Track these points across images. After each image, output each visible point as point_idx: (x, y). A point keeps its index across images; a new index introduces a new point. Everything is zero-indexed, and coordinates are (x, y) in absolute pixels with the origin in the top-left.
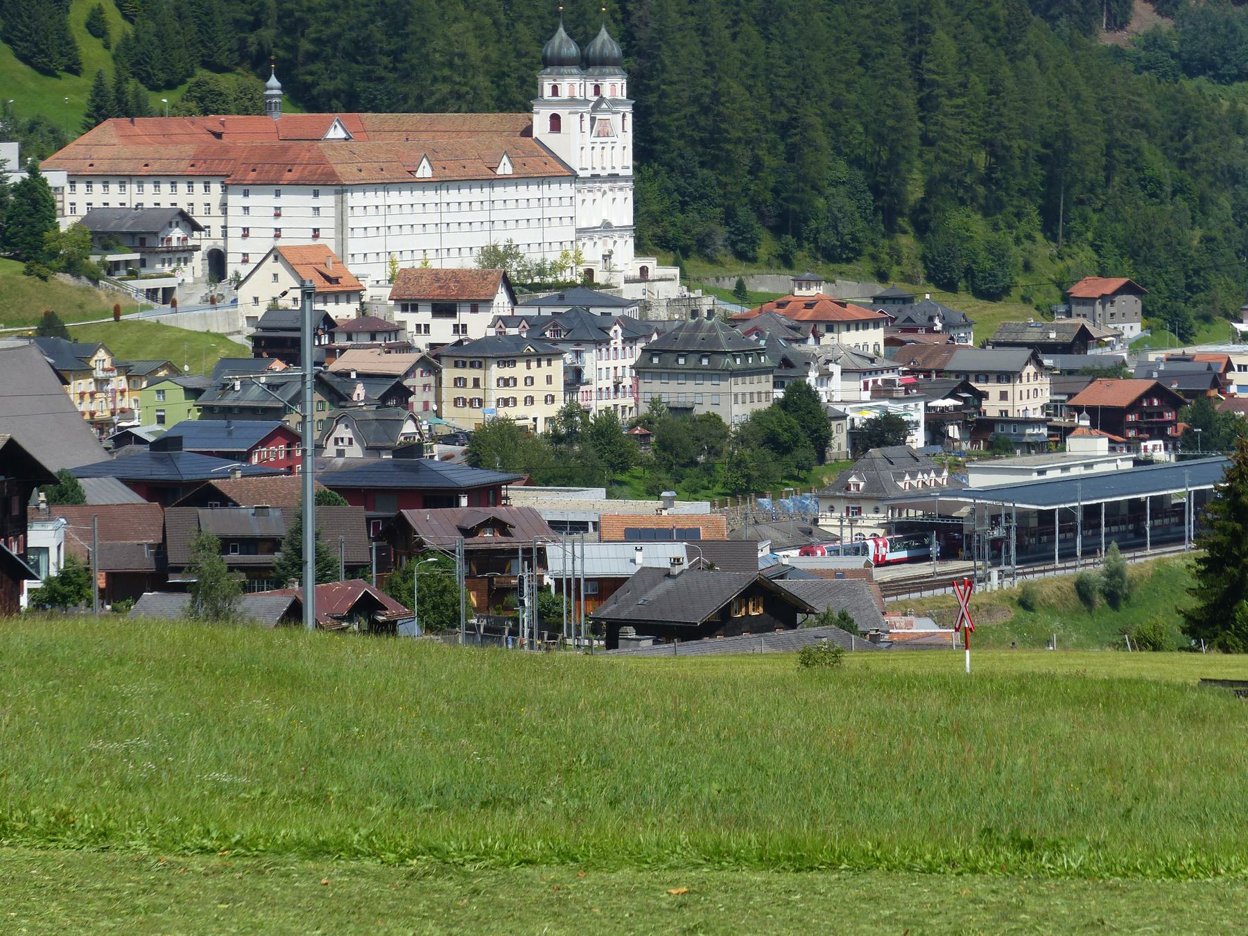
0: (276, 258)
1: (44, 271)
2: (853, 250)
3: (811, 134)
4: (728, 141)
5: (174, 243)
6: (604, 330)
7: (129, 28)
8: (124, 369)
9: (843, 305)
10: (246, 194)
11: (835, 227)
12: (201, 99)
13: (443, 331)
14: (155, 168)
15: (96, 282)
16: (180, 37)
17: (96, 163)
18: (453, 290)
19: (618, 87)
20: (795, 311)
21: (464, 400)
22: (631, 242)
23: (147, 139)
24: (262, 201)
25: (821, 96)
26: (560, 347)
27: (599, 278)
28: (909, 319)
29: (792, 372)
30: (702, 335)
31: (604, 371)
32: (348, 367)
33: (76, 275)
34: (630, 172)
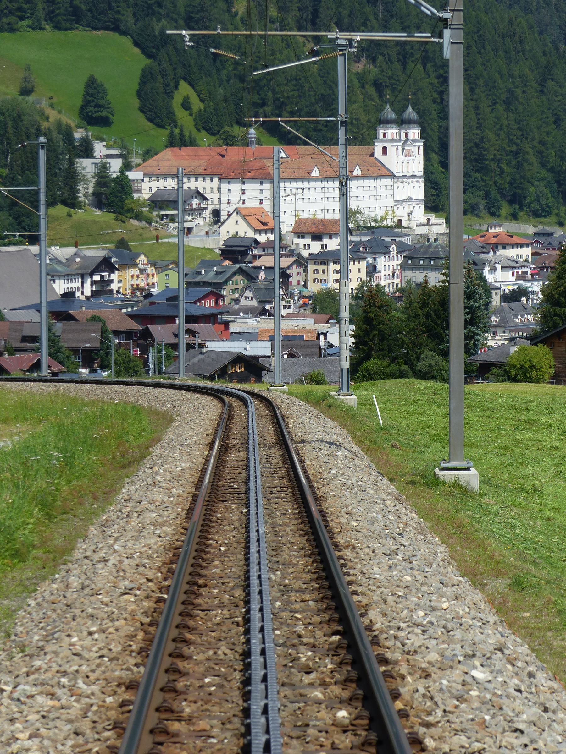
0: (237, 213)
1: (124, 218)
2: (547, 211)
3: (527, 156)
4: (486, 160)
5: (194, 206)
6: (387, 247)
7: (202, 106)
8: (153, 264)
9: (511, 236)
10: (229, 183)
11: (539, 201)
12: (225, 139)
13: (316, 247)
14: (163, 170)
15: (150, 223)
16: (226, 110)
17: (161, 169)
18: (321, 229)
19: (395, 134)
20: (489, 239)
21: (318, 280)
22: (423, 206)
23: (187, 157)
24: (236, 187)
25: (533, 139)
26: (366, 255)
27: (404, 224)
28: (550, 243)
29: (476, 268)
30: (431, 250)
31: (387, 267)
32: (261, 264)
33: (140, 220)
34: (422, 174)
